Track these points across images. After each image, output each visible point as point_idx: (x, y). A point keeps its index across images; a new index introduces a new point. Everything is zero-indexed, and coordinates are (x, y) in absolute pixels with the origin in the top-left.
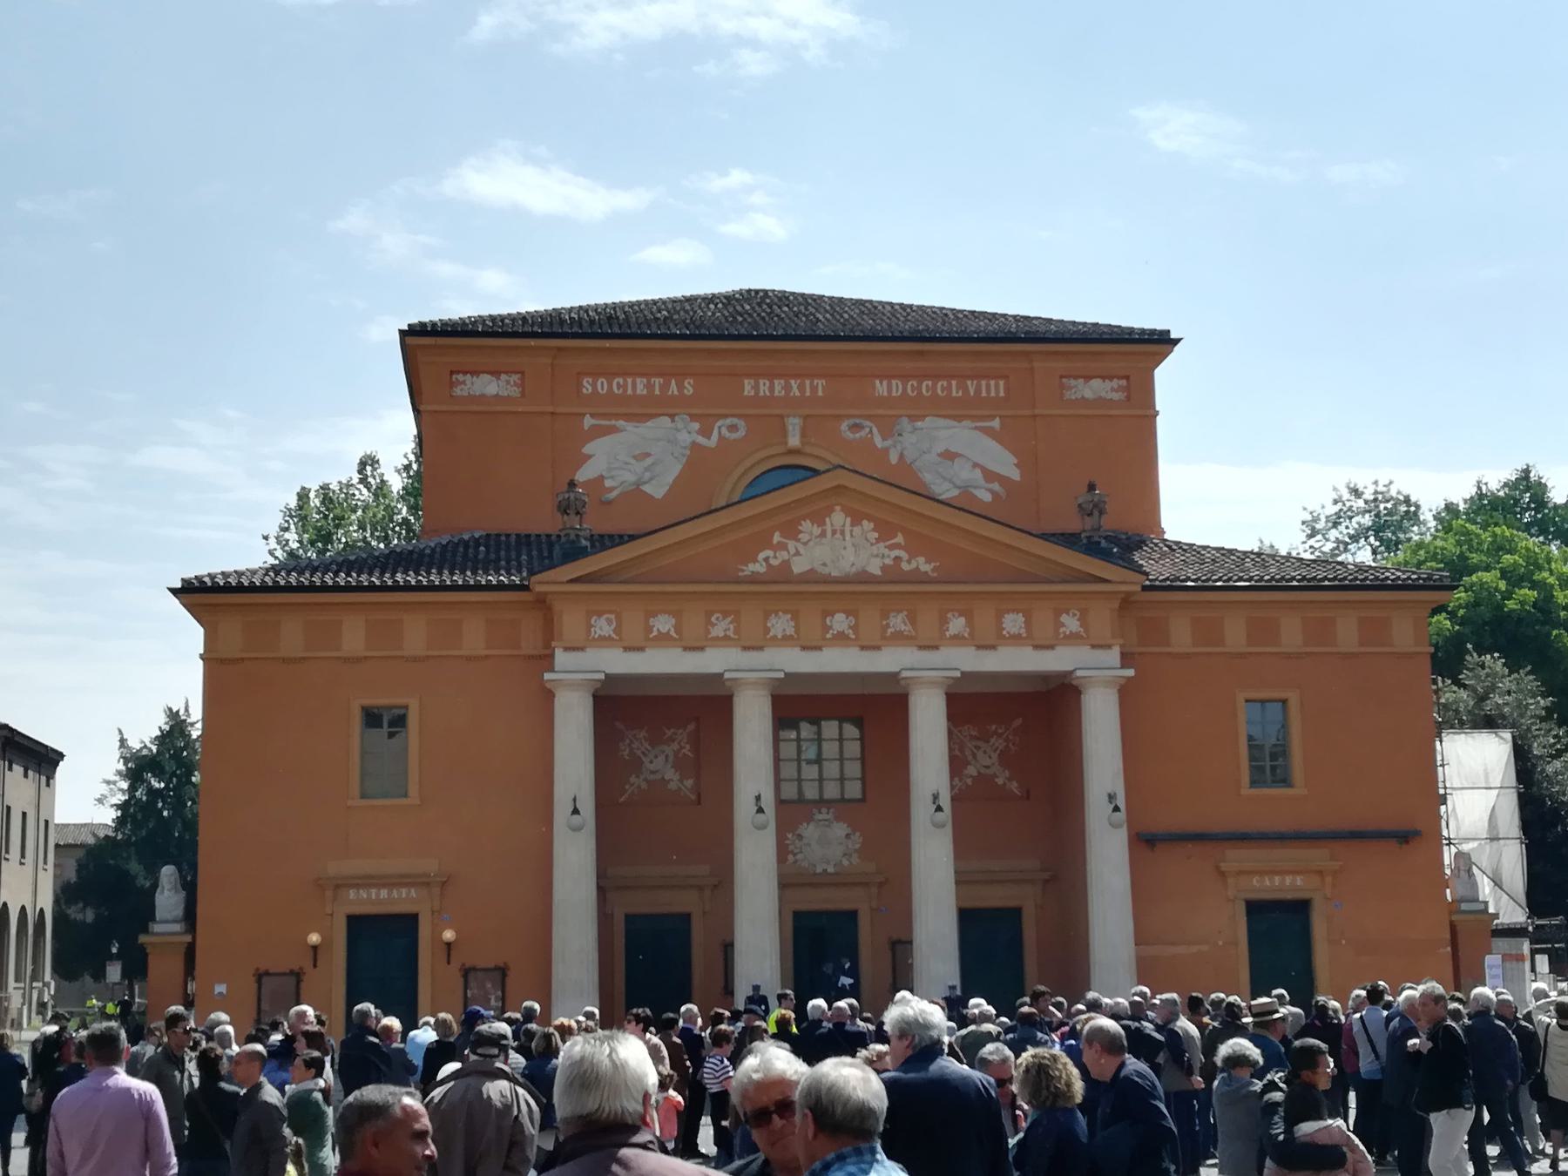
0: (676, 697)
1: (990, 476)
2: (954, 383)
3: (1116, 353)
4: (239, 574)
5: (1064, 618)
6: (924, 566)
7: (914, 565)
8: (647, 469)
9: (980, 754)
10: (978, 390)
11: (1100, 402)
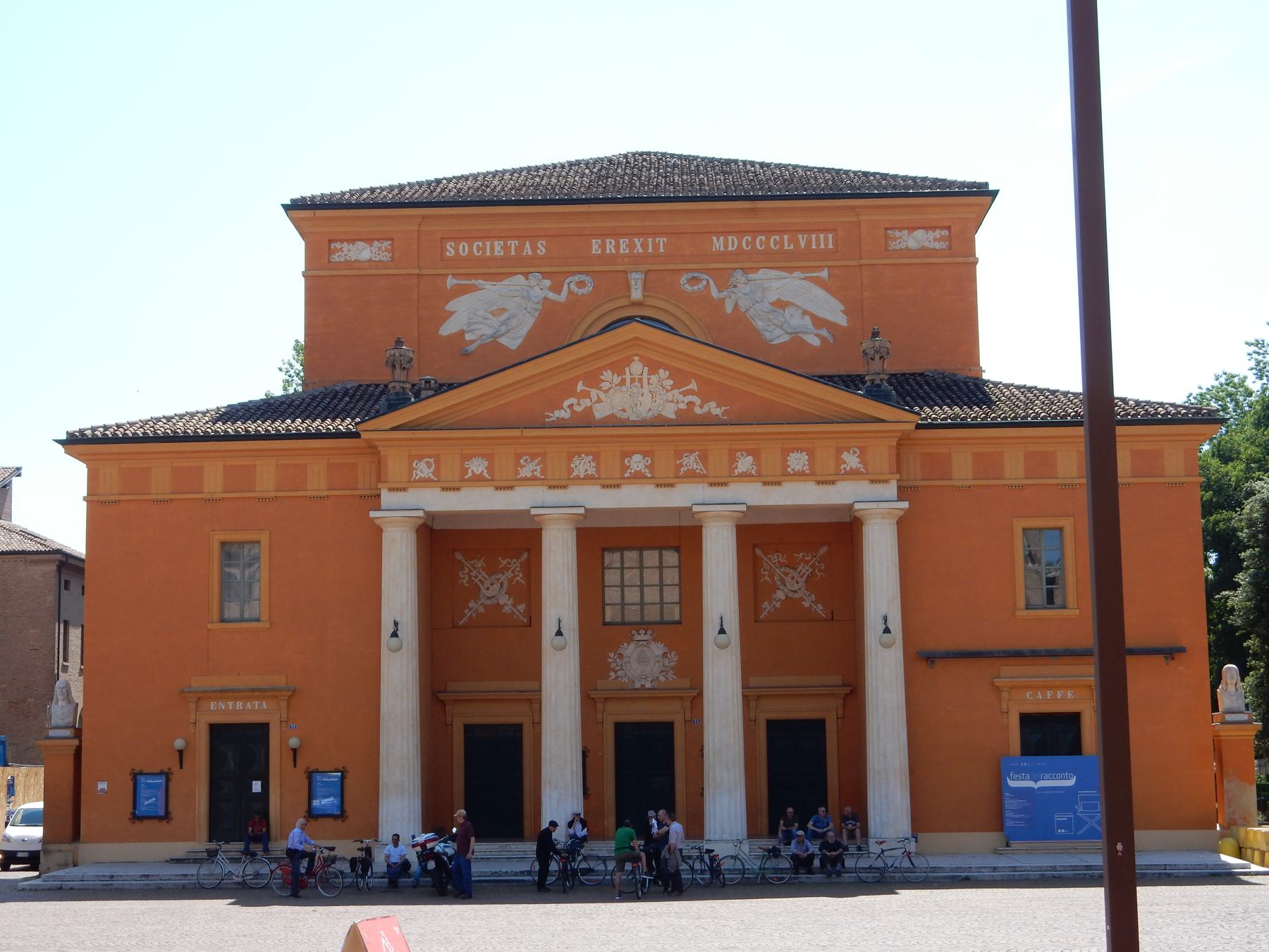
0: (513, 530)
1: (818, 322)
2: (786, 237)
3: (937, 205)
4: (106, 428)
5: (845, 456)
6: (714, 409)
7: (706, 409)
8: (503, 323)
9: (788, 580)
10: (809, 243)
11: (925, 252)
